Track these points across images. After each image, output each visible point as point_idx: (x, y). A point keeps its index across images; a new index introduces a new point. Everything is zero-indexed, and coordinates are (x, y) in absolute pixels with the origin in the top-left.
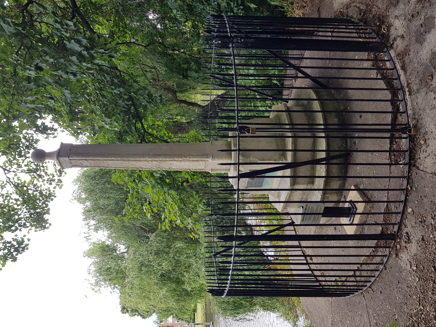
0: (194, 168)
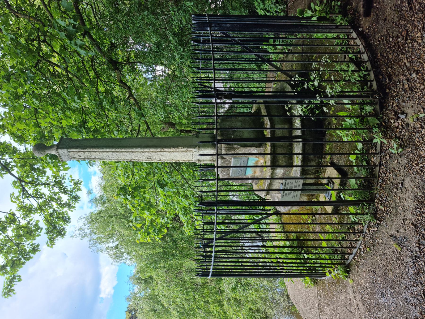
0: (183, 159)
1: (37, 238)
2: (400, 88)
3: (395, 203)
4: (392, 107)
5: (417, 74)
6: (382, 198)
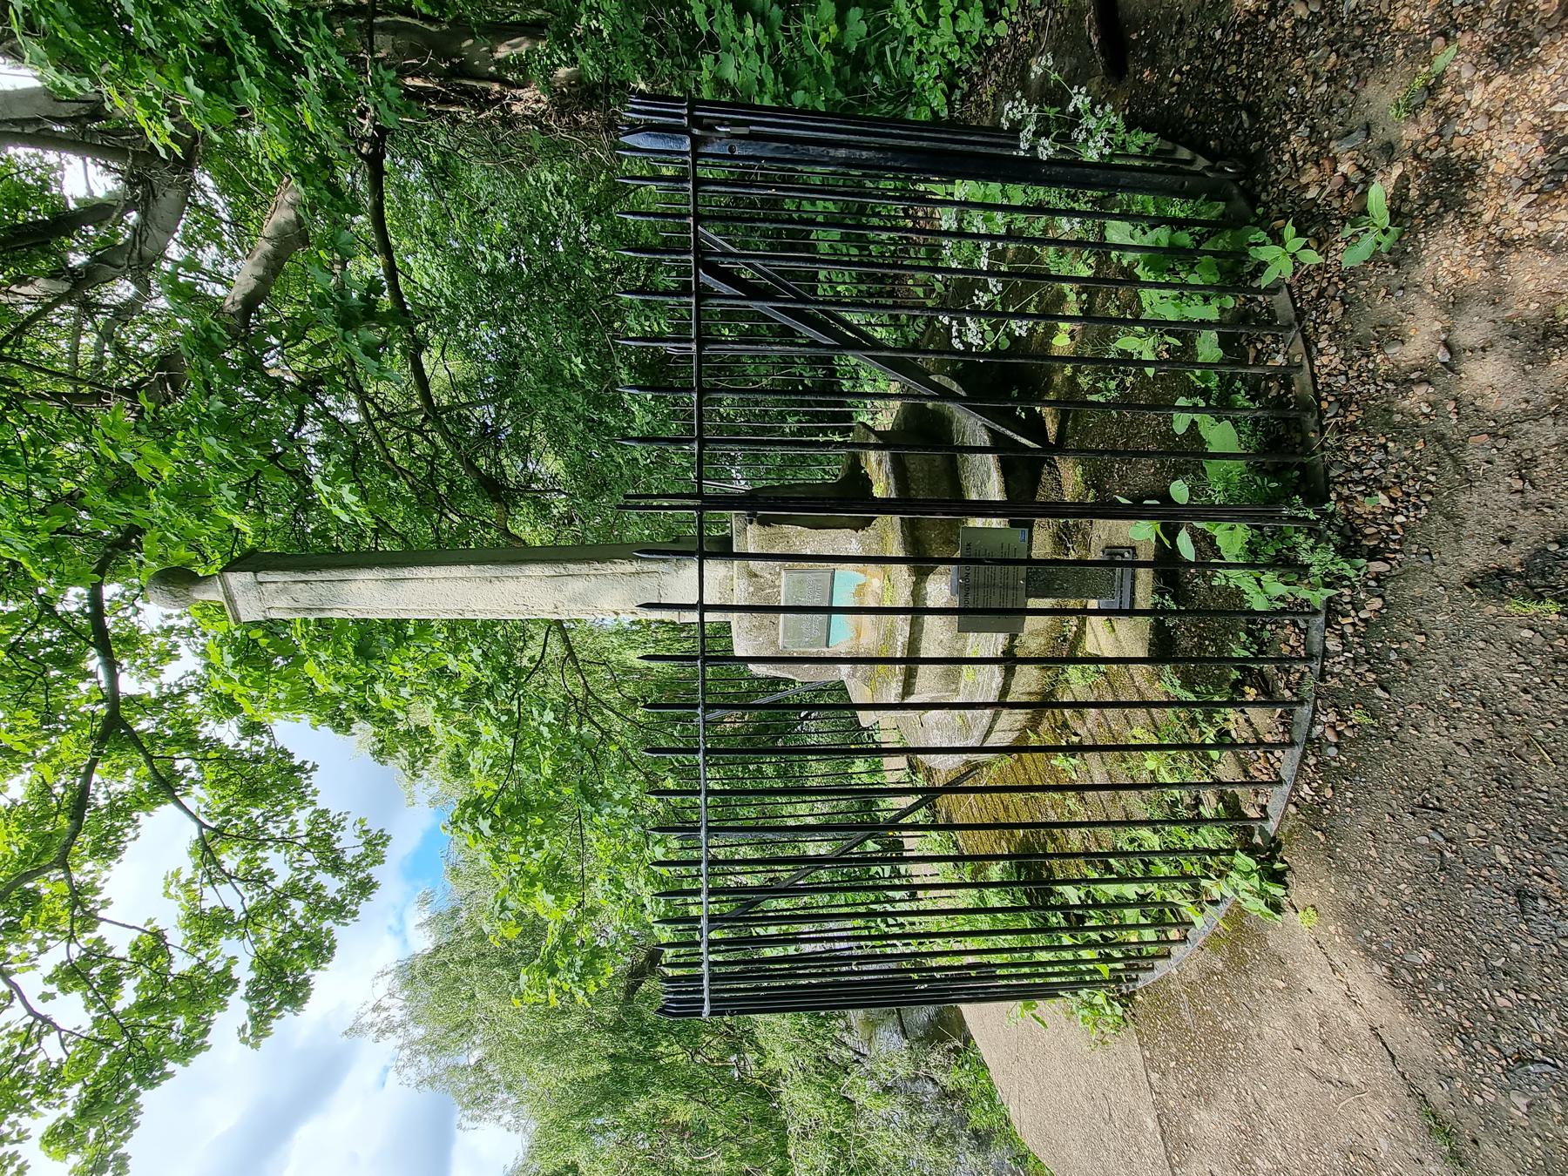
6: (1359, 467)
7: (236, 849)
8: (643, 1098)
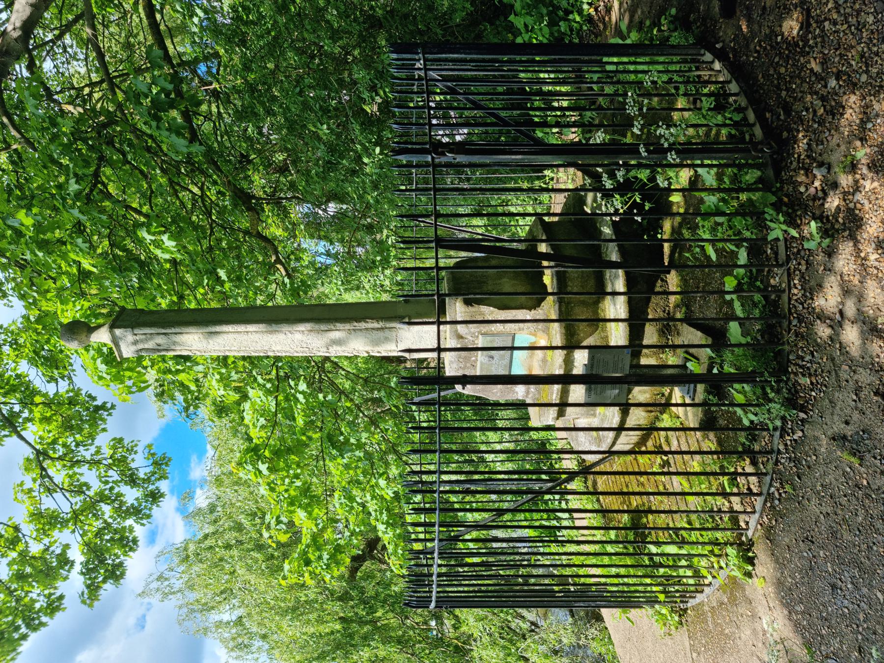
1: (59, 584)
2: (808, 122)
3: (833, 359)
4: (799, 162)
5: (837, 79)
6: (802, 358)
7: (59, 468)
8: (366, 649)
